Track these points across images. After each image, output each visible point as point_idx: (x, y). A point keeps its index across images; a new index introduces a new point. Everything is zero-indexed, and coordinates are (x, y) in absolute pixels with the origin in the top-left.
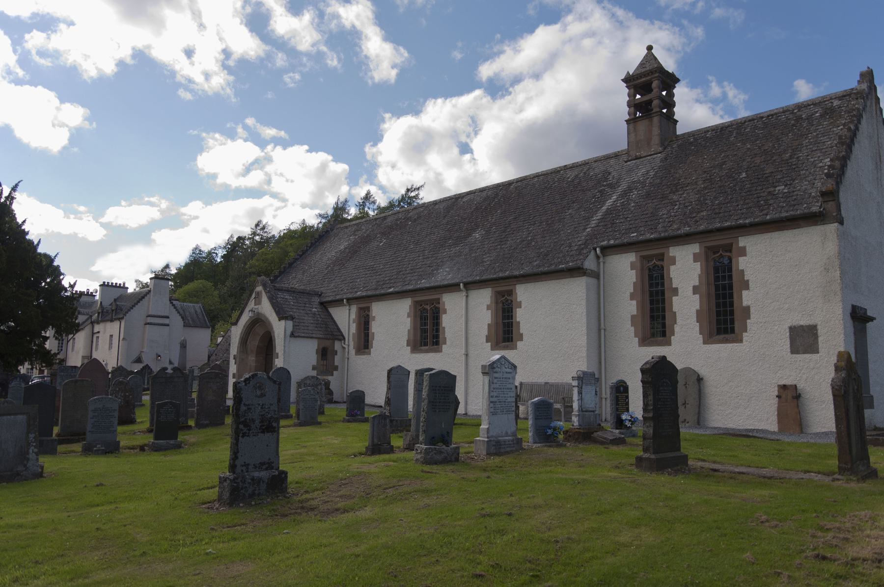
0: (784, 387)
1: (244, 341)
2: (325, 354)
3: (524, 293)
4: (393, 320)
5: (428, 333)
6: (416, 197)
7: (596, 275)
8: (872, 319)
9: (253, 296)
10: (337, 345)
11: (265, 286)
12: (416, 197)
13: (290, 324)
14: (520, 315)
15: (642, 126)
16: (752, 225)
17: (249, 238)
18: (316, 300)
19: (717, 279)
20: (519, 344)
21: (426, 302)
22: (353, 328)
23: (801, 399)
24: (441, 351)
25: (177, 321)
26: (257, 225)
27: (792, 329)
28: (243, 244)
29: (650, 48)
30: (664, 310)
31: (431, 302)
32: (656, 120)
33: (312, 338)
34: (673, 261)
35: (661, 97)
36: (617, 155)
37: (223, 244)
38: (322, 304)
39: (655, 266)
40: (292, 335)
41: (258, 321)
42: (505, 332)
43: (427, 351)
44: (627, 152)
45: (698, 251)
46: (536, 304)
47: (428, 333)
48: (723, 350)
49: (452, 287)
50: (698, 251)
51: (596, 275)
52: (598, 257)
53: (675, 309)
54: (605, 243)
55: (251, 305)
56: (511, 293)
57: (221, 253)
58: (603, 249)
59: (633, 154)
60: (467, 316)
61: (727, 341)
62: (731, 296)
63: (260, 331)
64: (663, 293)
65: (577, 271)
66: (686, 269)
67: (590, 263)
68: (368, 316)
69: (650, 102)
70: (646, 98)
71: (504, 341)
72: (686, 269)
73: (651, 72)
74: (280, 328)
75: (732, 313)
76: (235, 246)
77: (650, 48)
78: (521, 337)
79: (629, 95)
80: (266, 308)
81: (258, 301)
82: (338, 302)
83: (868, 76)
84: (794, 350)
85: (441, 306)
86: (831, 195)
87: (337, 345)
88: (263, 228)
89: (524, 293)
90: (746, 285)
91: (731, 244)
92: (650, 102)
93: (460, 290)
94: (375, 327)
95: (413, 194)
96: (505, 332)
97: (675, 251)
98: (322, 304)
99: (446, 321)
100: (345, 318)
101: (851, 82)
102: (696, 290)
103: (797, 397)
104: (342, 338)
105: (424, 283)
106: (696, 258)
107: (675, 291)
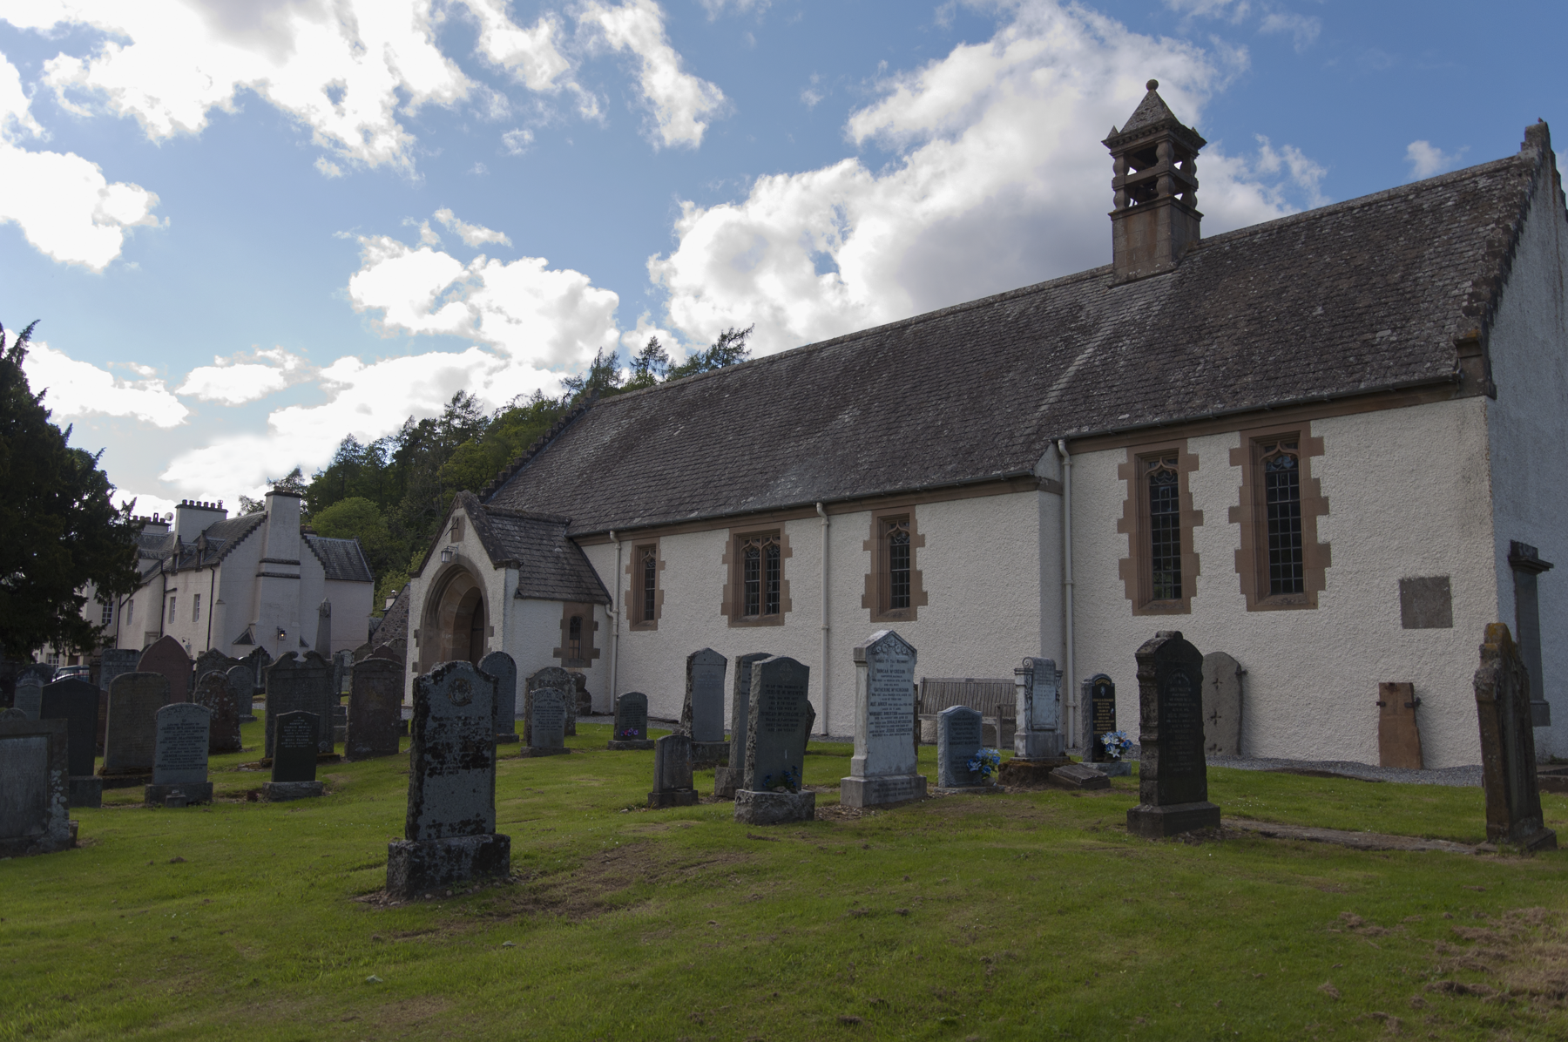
0: (1390, 688)
1: (433, 605)
2: (576, 628)
3: (929, 520)
4: (697, 569)
5: (758, 591)
6: (738, 350)
7: (1057, 488)
8: (1546, 566)
9: (449, 525)
10: (598, 613)
11: (469, 508)
12: (738, 350)
13: (514, 574)
14: (923, 559)
15: (1139, 223)
16: (1334, 400)
17: (442, 423)
18: (561, 533)
19: (1271, 495)
20: (921, 610)
21: (755, 536)
22: (627, 583)
23: (1421, 708)
24: (780, 623)
25: (313, 569)
26: (456, 400)
27: (1405, 584)
28: (432, 433)
29: (1152, 85)
30: (1177, 550)
31: (765, 536)
32: (1163, 213)
33: (552, 599)
34: (1194, 464)
35: (1172, 173)
36: (1093, 276)
37: (395, 433)
38: (570, 539)
39: (1162, 472)
40: (519, 595)
41: (457, 570)
42: (896, 589)
43: (758, 624)
44: (1113, 270)
45: (1237, 445)
46: (950, 539)
47: (758, 591)
48: (1282, 621)
49: (802, 510)
50: (1237, 445)
51: (1057, 488)
52: (1060, 457)
53: (1197, 548)
54: (1073, 431)
55: (446, 541)
56: (906, 519)
57: (392, 448)
58: (1070, 442)
59: (1123, 272)
60: (828, 562)
61: (1289, 605)
62: (1297, 525)
63: (460, 587)
64: (1176, 521)
65: (1022, 481)
66: (1216, 478)
67: (1046, 468)
68: (653, 560)
69: (1152, 181)
70: (1147, 174)
71: (894, 606)
72: (1216, 478)
73: (1155, 128)
74: (496, 583)
75: (1298, 555)
76: (417, 437)
77: (1152, 85)
78: (924, 598)
79: (1115, 169)
80: (472, 547)
81: (458, 535)
82: (600, 537)
83: (1539, 136)
84: (1409, 622)
85: (782, 543)
86: (1473, 346)
87: (598, 613)
88: (467, 405)
89: (929, 520)
90: (1323, 507)
91: (1297, 434)
92: (1152, 181)
93: (816, 515)
94: (665, 581)
95: (732, 345)
96: (896, 589)
97: (1197, 446)
98: (570, 539)
99: (791, 569)
100: (612, 565)
101: (1509, 146)
102: (1234, 514)
103: (1415, 704)
104: (606, 600)
105: (752, 503)
106: (1235, 458)
107: (1198, 517)
